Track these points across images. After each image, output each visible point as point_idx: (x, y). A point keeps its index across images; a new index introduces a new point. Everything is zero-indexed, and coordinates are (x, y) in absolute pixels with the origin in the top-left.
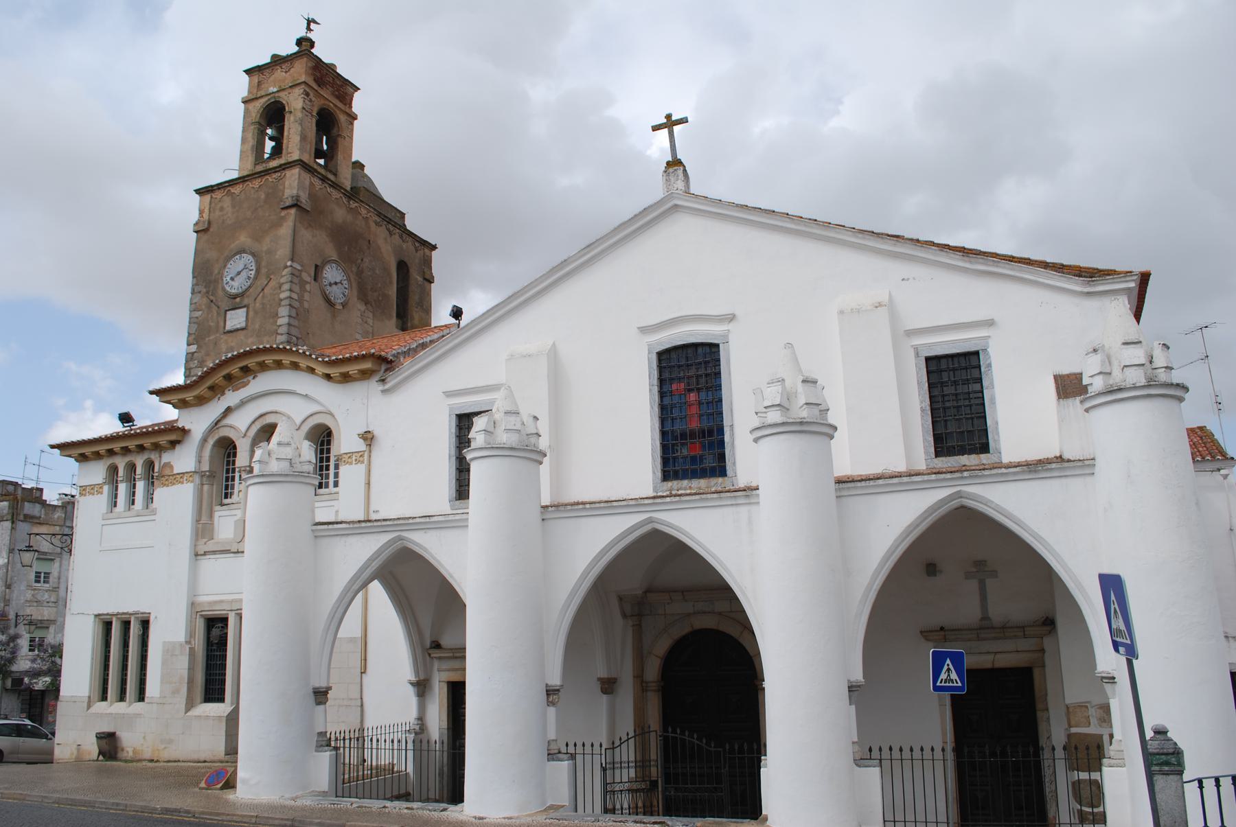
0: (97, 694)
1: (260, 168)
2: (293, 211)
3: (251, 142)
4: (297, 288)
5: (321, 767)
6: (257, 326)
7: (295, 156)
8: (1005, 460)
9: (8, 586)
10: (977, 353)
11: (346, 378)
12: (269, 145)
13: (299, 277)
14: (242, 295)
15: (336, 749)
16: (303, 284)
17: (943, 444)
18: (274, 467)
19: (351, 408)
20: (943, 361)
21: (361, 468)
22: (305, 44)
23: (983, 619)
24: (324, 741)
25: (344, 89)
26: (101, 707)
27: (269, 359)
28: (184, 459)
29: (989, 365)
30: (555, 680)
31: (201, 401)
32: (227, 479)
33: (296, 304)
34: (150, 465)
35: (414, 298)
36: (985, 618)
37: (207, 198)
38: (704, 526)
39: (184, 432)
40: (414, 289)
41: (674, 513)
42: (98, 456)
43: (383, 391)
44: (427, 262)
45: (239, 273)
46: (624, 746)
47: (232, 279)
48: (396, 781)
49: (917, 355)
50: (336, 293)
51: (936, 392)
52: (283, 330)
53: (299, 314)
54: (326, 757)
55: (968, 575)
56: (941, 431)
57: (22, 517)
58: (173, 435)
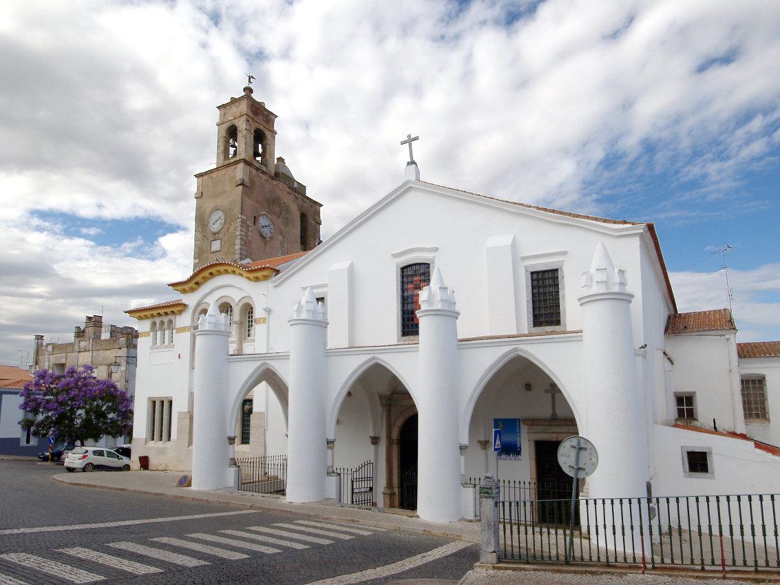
0: (150, 438)
1: (226, 162)
2: (241, 187)
3: (222, 148)
4: (244, 229)
5: (231, 475)
6: (226, 249)
7: (243, 156)
8: (568, 330)
9: (127, 382)
10: (557, 270)
11: (257, 279)
12: (232, 150)
13: (246, 223)
14: (218, 233)
15: (339, 475)
16: (248, 227)
17: (405, 333)
18: (207, 327)
19: (260, 294)
20: (540, 274)
21: (265, 325)
22: (248, 90)
23: (552, 415)
24: (234, 462)
25: (269, 117)
26: (152, 444)
27: (222, 268)
28: (184, 320)
29: (563, 277)
30: (465, 440)
31: (192, 290)
32: (249, 326)
33: (245, 238)
34: (170, 322)
35: (310, 234)
36: (554, 413)
37: (201, 178)
38: (547, 354)
39: (185, 306)
40: (310, 228)
41: (531, 346)
42: (146, 317)
43: (274, 286)
44: (318, 213)
45: (217, 221)
46: (363, 468)
47: (214, 224)
48: (279, 483)
49: (526, 271)
50: (266, 232)
51: (535, 291)
52: (238, 252)
53: (246, 243)
54: (233, 470)
55: (546, 391)
56: (537, 312)
57: (132, 346)
58: (179, 308)
